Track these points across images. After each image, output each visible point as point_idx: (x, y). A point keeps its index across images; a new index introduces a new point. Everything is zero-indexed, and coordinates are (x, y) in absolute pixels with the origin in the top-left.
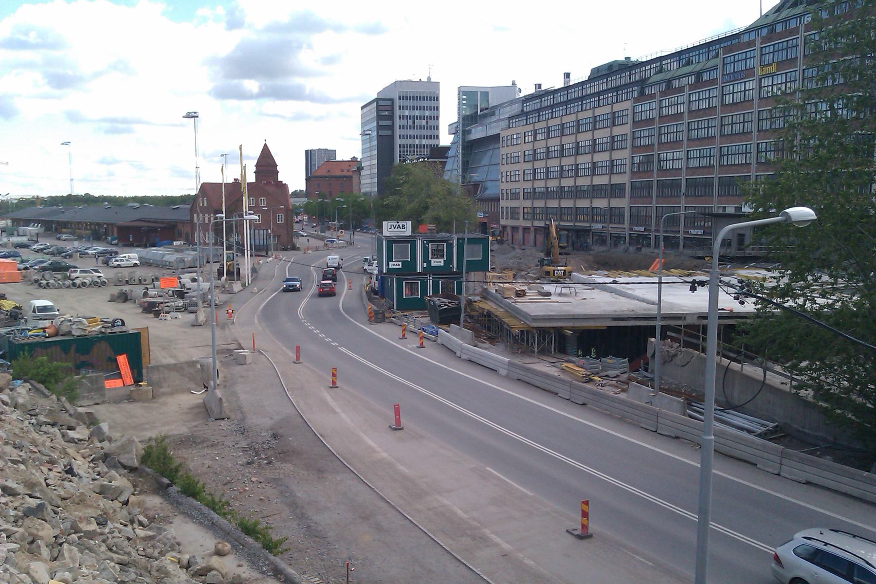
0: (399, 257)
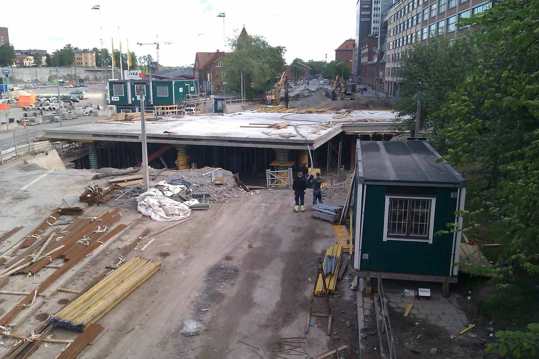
0: (118, 93)
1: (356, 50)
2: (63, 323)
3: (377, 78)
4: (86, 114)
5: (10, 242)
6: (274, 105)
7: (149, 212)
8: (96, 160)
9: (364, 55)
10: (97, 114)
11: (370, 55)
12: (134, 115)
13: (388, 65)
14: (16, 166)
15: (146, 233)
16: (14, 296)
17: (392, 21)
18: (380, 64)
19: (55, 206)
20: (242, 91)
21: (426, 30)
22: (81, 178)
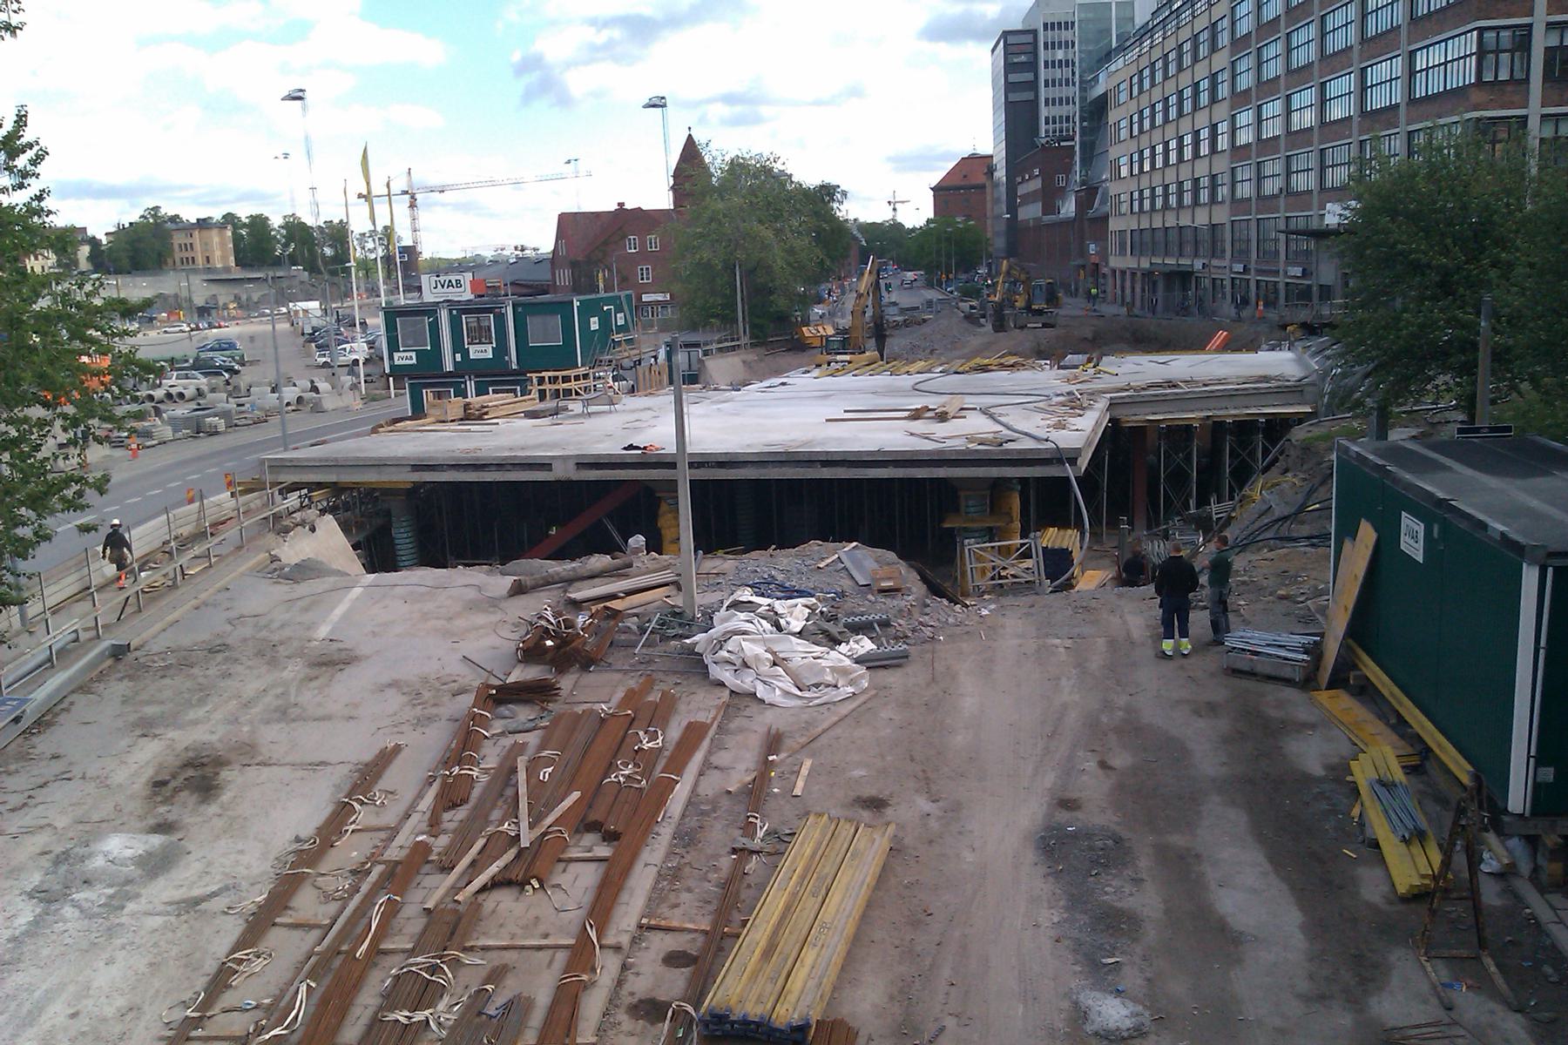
0: (410, 342)
1: (996, 185)
2: (745, 1022)
3: (1079, 262)
4: (290, 408)
5: (392, 793)
6: (854, 353)
7: (746, 682)
8: (412, 539)
9: (1029, 198)
10: (321, 407)
11: (1050, 197)
12: (490, 404)
13: (1114, 225)
14: (251, 569)
15: (774, 742)
16: (525, 953)
17: (1123, 97)
18: (1086, 224)
19: (453, 678)
20: (740, 319)
21: (1245, 118)
22: (472, 594)
